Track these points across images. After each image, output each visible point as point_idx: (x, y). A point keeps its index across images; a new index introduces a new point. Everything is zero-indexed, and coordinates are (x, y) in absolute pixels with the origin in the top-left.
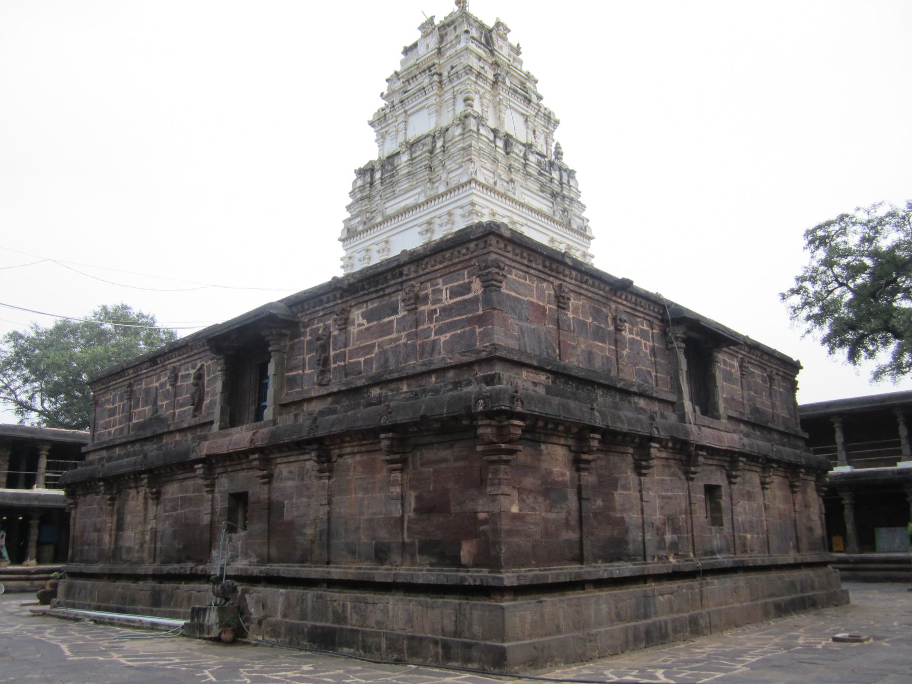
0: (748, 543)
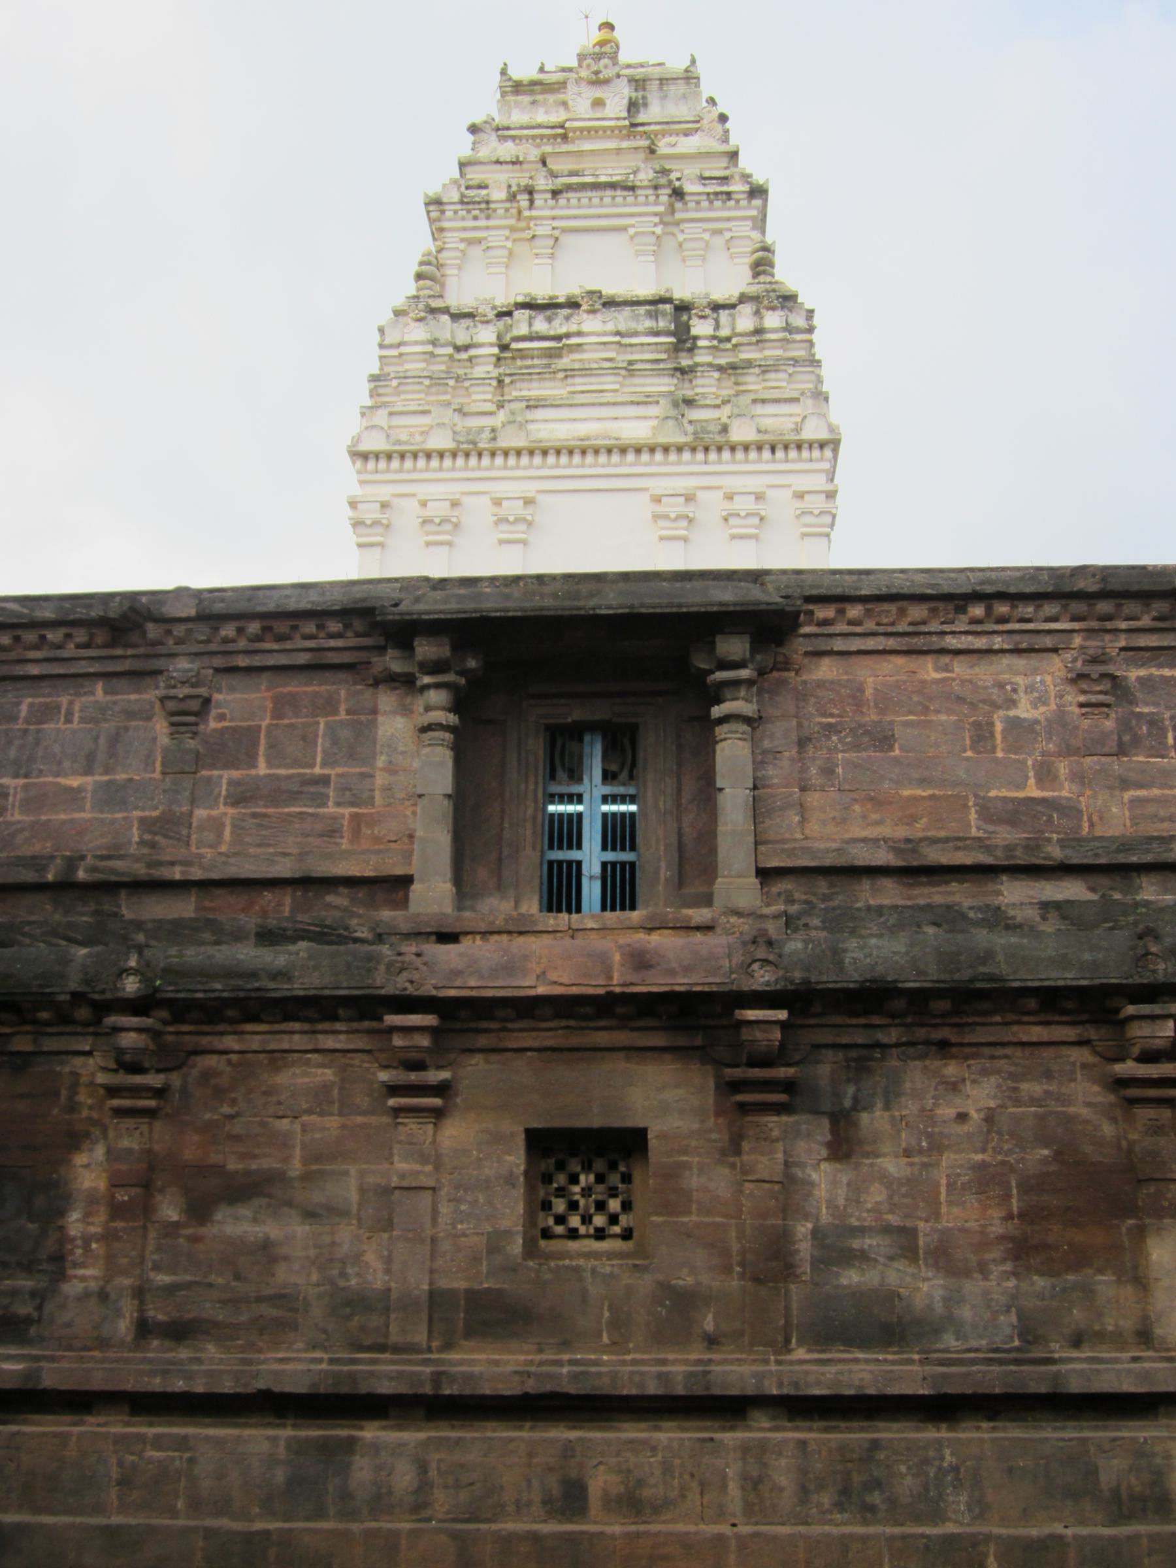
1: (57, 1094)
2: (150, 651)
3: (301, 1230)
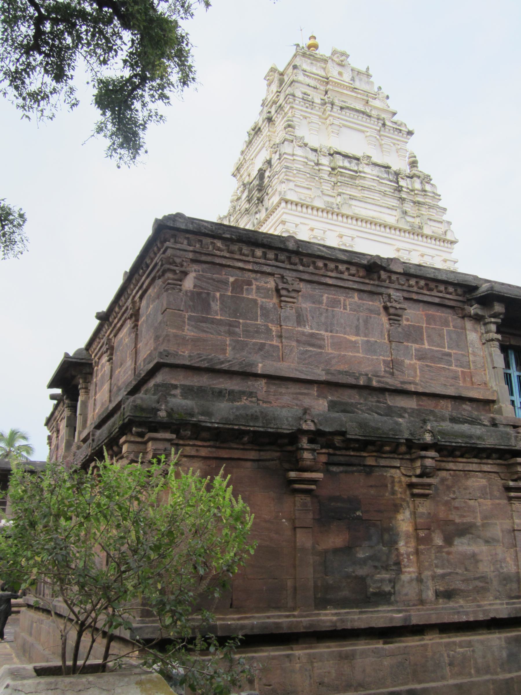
1: (386, 486)
2: (380, 283)
3: (485, 548)
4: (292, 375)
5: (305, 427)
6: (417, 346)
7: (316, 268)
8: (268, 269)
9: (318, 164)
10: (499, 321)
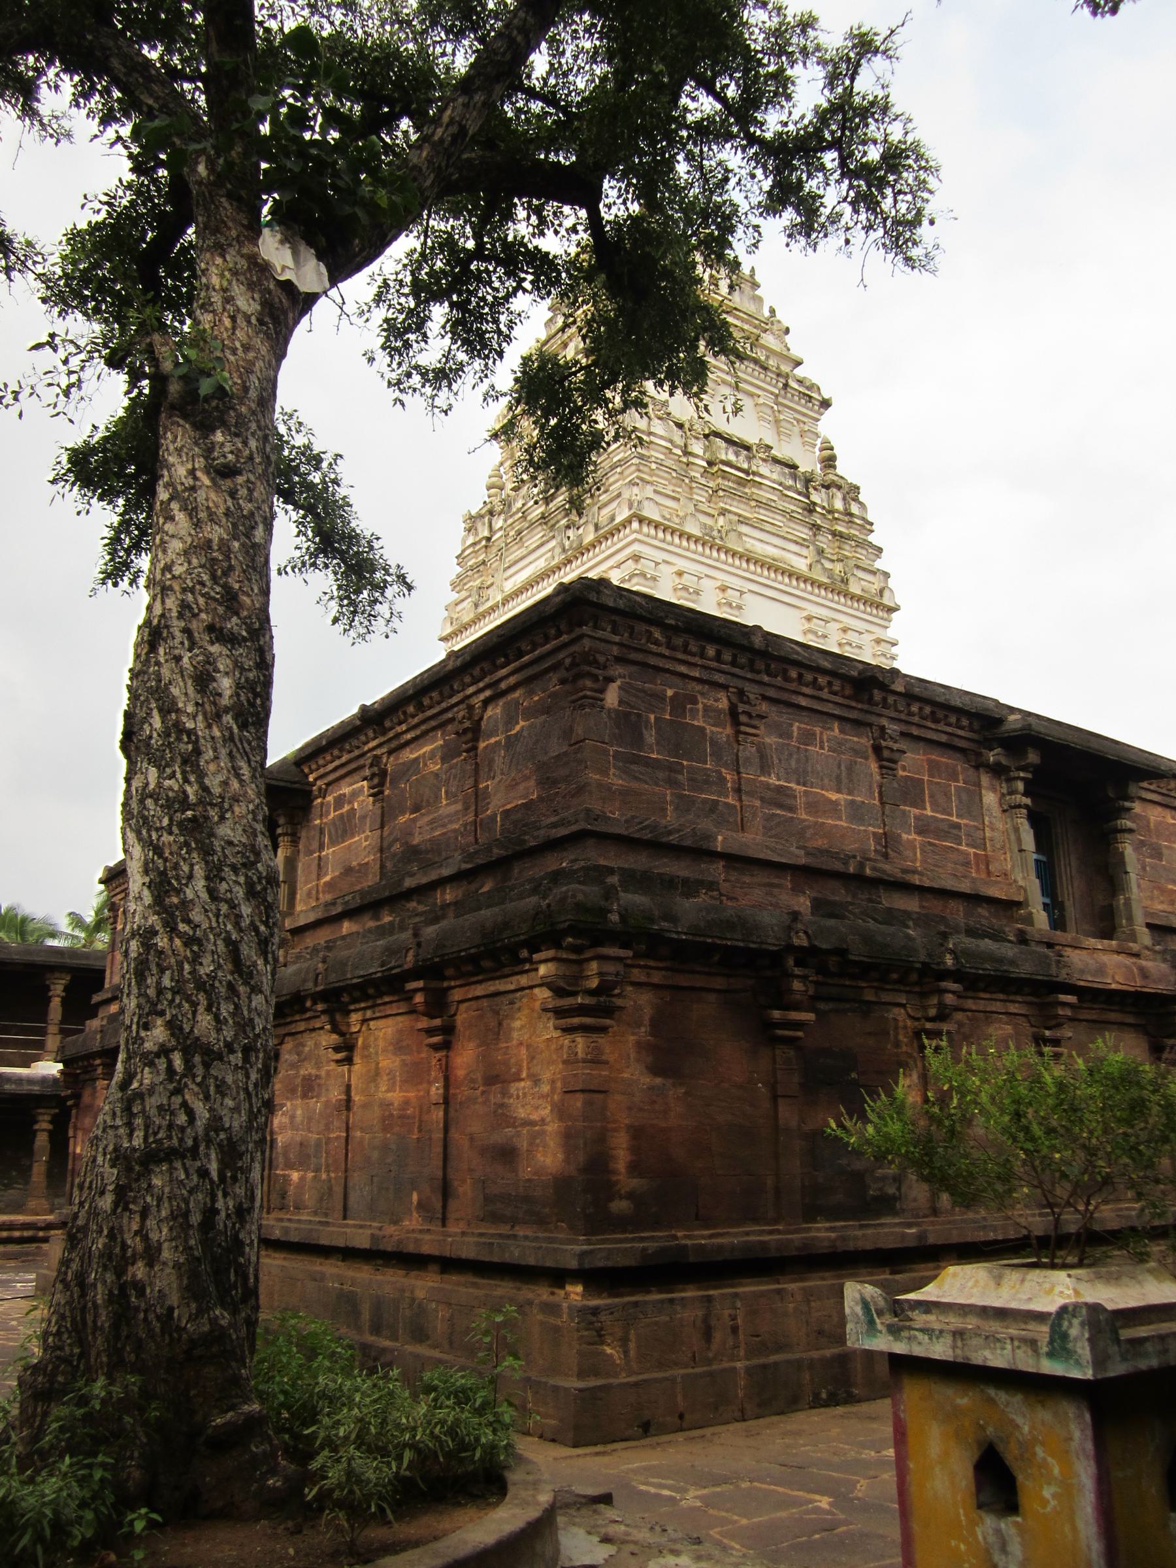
0: (291, 1190)
4: (761, 856)
5: (796, 942)
6: (917, 811)
7: (787, 679)
8: (720, 678)
9: (687, 453)
10: (1030, 776)
